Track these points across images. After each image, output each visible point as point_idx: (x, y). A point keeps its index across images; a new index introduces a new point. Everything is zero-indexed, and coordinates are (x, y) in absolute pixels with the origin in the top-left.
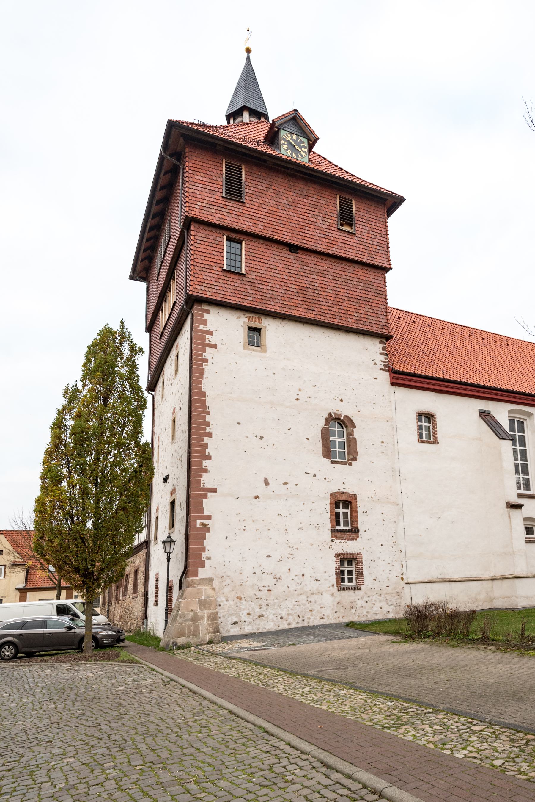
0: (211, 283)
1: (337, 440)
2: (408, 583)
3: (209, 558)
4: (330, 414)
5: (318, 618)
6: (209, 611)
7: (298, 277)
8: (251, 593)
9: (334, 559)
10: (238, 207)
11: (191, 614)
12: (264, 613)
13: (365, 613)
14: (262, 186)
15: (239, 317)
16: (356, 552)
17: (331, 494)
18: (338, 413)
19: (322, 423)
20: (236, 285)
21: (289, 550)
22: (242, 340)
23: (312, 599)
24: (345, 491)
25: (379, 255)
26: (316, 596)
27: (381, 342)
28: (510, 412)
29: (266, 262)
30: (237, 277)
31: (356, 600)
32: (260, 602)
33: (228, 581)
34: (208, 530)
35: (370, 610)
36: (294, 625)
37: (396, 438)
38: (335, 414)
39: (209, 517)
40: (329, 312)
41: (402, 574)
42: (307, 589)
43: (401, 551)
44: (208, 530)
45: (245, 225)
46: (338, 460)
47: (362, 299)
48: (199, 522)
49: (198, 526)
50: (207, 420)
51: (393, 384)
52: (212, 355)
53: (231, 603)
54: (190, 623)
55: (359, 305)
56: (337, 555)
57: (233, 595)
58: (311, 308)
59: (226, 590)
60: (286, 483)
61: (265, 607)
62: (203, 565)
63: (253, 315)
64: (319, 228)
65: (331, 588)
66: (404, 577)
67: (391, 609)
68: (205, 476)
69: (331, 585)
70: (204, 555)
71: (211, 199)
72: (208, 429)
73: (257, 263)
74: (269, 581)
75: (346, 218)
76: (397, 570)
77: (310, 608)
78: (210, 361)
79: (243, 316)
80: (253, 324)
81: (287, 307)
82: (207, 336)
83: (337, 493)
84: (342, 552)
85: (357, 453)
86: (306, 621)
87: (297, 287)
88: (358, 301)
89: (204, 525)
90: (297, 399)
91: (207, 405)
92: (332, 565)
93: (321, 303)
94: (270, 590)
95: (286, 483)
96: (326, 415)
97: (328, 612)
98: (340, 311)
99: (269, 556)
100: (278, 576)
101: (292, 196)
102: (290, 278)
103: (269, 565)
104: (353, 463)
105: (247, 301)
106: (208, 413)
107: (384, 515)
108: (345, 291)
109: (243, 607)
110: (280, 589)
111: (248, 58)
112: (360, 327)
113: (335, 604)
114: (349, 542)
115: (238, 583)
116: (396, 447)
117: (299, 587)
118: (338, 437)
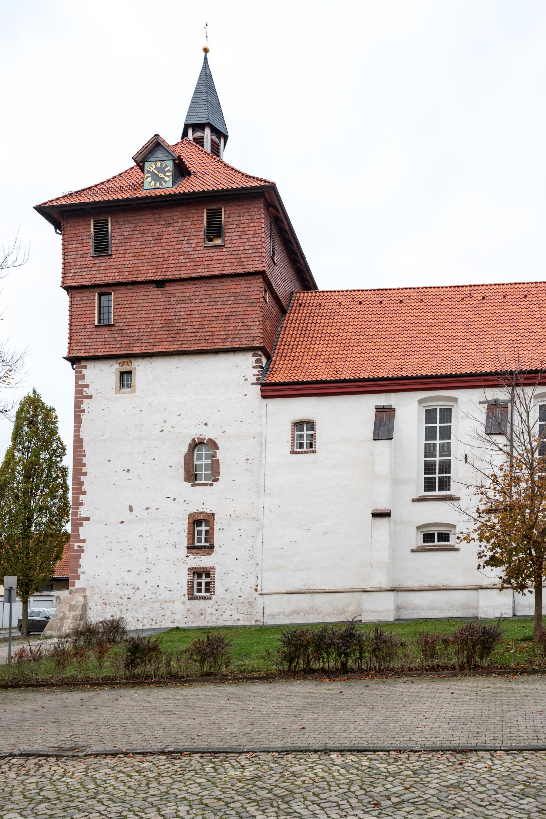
0: (84, 341)
1: (203, 463)
2: (261, 594)
3: (84, 573)
4: (194, 439)
5: (169, 622)
6: (75, 613)
7: (164, 311)
8: (115, 600)
9: (187, 572)
10: (106, 261)
11: (62, 614)
12: (124, 616)
13: (214, 620)
14: (127, 229)
15: (112, 365)
16: (209, 566)
17: (190, 515)
18: (202, 437)
19: (185, 449)
20: (106, 336)
21: (147, 566)
22: (114, 387)
23: (165, 606)
24: (203, 511)
25: (251, 259)
26: (168, 604)
27: (254, 356)
28: (420, 402)
29: (133, 305)
30: (106, 329)
31: (206, 608)
32: (121, 607)
33: (97, 591)
34: (83, 551)
35: (220, 617)
36: (148, 627)
37: (263, 453)
38: (198, 438)
39: (84, 541)
40: (194, 338)
41: (257, 586)
42: (161, 598)
43: (257, 564)
44: (83, 551)
45: (113, 276)
46: (203, 482)
47: (231, 314)
48: (76, 545)
49: (75, 548)
50: (84, 462)
51: (263, 397)
52: (88, 406)
53: (99, 607)
54: (58, 621)
55: (228, 321)
56: (190, 569)
57: (100, 601)
58: (176, 339)
59: (96, 597)
60: (148, 508)
61: (125, 611)
62: (78, 578)
63: (124, 360)
64: (183, 254)
65: (183, 597)
66: (258, 588)
67: (241, 617)
68: (81, 508)
69: (182, 594)
70: (80, 570)
71: (83, 263)
72: (84, 470)
73: (125, 310)
74: (128, 591)
75: (214, 230)
76: (251, 582)
77: (163, 614)
78: (86, 411)
79: (115, 363)
80: (125, 368)
81: (152, 344)
82: (85, 389)
83: (195, 513)
84: (195, 566)
85: (219, 473)
86: (159, 624)
87: (162, 322)
88: (227, 318)
89: (80, 547)
90: (162, 431)
91: (84, 449)
92: (184, 577)
93: (187, 331)
94: (129, 598)
95: (148, 508)
96: (189, 441)
97: (178, 617)
98: (206, 334)
99: (129, 571)
100: (136, 587)
101: (157, 229)
102: (156, 315)
103: (129, 578)
104: (214, 483)
105: (115, 349)
106: (84, 456)
107: (242, 531)
108: (212, 311)
109: (108, 611)
110: (137, 597)
111: (206, 59)
112: (228, 345)
113: (186, 610)
114: (203, 557)
115: (105, 592)
116: (263, 462)
117: (154, 596)
118: (200, 461)
